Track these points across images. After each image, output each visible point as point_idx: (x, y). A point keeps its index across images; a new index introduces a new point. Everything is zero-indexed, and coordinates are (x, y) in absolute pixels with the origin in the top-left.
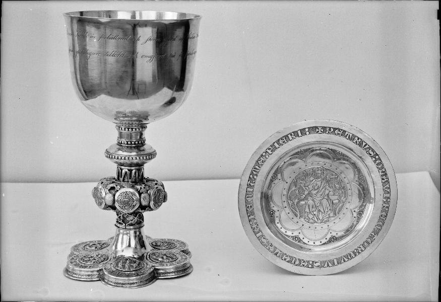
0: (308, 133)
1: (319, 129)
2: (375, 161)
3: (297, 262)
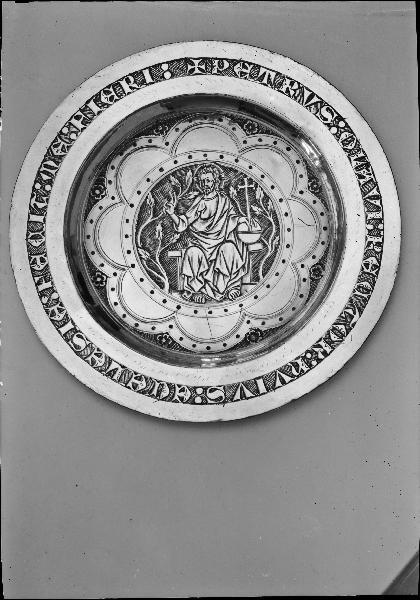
0: (168, 75)
1: (193, 64)
2: (337, 136)
3: (166, 392)
